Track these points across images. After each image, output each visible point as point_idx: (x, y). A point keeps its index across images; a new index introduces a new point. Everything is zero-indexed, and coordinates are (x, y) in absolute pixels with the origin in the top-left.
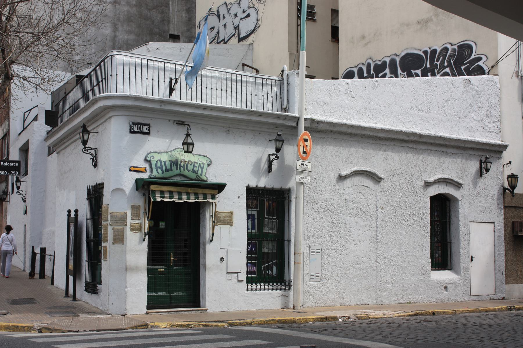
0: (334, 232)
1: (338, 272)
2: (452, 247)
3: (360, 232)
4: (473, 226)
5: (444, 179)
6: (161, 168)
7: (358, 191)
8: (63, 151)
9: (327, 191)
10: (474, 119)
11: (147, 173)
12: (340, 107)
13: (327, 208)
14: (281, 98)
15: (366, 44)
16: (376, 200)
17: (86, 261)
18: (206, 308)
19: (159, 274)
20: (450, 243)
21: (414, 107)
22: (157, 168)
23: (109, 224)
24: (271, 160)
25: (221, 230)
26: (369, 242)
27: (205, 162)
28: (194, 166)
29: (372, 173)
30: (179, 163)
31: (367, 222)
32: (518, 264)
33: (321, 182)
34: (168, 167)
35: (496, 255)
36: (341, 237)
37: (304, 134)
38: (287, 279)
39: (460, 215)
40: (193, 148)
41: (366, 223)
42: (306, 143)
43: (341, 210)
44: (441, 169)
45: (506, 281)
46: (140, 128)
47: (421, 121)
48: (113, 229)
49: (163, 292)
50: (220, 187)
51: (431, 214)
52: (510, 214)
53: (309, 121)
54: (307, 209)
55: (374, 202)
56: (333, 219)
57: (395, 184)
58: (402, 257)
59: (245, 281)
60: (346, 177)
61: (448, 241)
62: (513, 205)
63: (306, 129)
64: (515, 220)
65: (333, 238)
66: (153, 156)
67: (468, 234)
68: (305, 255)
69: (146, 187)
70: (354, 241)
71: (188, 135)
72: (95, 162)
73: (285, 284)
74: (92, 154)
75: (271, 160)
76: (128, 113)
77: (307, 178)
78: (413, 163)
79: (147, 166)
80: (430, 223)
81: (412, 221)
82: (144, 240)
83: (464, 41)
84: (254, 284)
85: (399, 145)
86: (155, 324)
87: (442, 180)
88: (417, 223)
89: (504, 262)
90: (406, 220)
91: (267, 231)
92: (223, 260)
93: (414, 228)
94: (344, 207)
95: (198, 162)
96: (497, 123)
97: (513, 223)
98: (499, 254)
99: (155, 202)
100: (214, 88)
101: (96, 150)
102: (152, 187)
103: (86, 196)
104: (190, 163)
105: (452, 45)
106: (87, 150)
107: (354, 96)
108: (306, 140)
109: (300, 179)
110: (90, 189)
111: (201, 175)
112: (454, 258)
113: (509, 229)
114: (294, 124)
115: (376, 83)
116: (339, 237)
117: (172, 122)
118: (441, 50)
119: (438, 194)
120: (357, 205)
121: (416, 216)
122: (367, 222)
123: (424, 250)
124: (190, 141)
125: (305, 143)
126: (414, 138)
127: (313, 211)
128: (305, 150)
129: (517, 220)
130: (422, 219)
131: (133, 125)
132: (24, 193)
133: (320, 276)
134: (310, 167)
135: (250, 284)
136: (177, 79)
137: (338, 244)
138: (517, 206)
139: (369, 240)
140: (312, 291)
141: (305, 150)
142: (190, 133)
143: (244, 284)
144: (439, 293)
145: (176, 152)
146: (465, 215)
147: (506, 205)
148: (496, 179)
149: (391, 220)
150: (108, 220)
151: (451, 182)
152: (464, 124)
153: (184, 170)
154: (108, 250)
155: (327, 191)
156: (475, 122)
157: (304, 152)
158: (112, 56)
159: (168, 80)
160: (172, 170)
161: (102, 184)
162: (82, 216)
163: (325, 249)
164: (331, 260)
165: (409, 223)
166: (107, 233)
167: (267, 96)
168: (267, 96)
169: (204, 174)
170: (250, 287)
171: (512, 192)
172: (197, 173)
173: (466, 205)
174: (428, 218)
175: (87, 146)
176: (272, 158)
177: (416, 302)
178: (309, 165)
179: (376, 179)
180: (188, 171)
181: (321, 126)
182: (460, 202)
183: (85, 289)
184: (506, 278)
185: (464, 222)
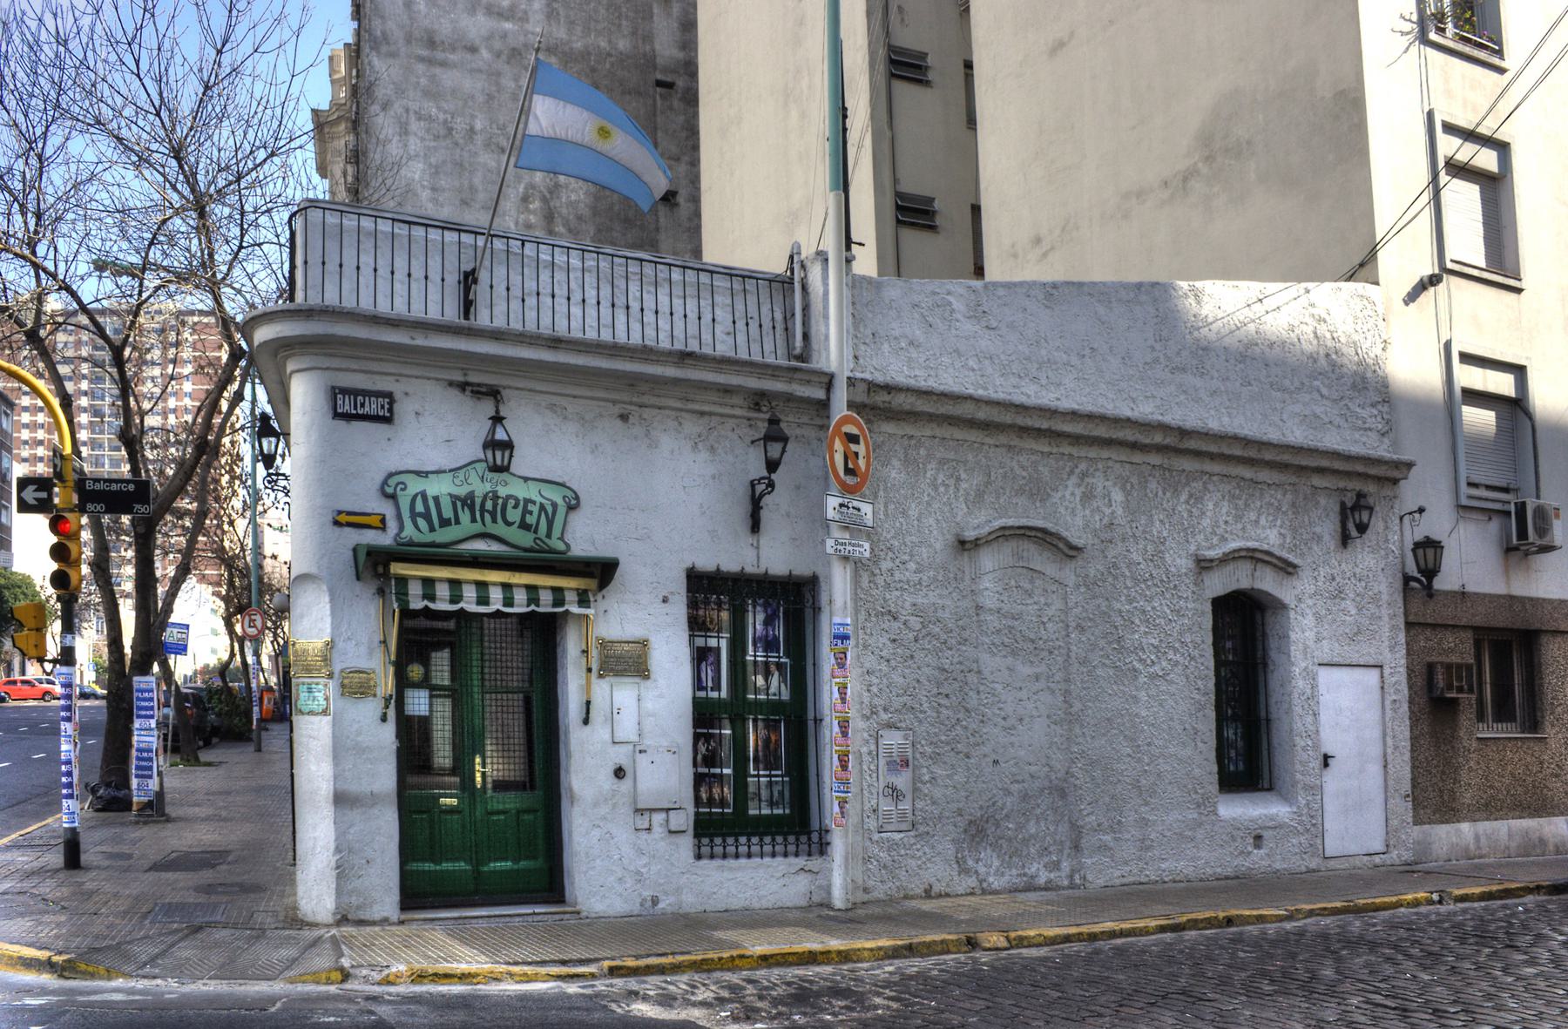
0: (947, 696)
1: (961, 805)
2: (1274, 731)
3: (1023, 694)
4: (1325, 675)
5: (1248, 550)
6: (427, 516)
10: (1322, 396)
11: (389, 530)
14: (786, 329)
15: (1045, 255)
18: (578, 908)
20: (1268, 720)
21: (1162, 360)
22: (414, 515)
24: (757, 494)
26: (1048, 722)
27: (560, 501)
28: (526, 512)
29: (1051, 534)
30: (478, 501)
31: (1042, 669)
32: (1443, 773)
33: (906, 557)
34: (448, 513)
35: (1389, 751)
36: (967, 710)
37: (845, 420)
38: (815, 825)
39: (1292, 648)
40: (511, 456)
41: (1038, 670)
42: (854, 447)
43: (966, 634)
44: (1240, 526)
45: (1414, 816)
46: (363, 405)
47: (1182, 397)
49: (457, 859)
50: (602, 572)
51: (1215, 644)
52: (1422, 644)
53: (862, 387)
54: (868, 631)
55: (1059, 613)
56: (944, 661)
57: (1115, 565)
58: (1139, 760)
59: (691, 831)
60: (976, 544)
61: (1263, 714)
62: (1429, 621)
63: (851, 405)
64: (1434, 659)
66: (402, 483)
67: (1313, 697)
68: (866, 758)
70: (1004, 719)
71: (497, 419)
73: (809, 839)
75: (757, 494)
76: (327, 362)
77: (859, 546)
78: (1165, 510)
80: (1213, 668)
81: (1164, 664)
84: (718, 840)
85: (1124, 458)
86: (394, 970)
87: (1243, 554)
88: (1179, 669)
89: (1408, 769)
90: (1149, 662)
93: (1171, 682)
94: (974, 626)
95: (539, 499)
96: (1380, 407)
97: (1431, 667)
98: (1396, 748)
100: (591, 301)
102: (398, 569)
107: (994, 325)
108: (853, 439)
109: (839, 547)
112: (1280, 759)
113: (1420, 681)
114: (820, 394)
116: (963, 710)
119: (1234, 592)
121: (1176, 651)
122: (1042, 669)
123: (1199, 739)
124: (500, 435)
125: (851, 445)
126: (1165, 438)
127: (884, 640)
128: (850, 466)
129: (1440, 659)
130: (1192, 658)
133: (910, 815)
134: (870, 516)
135: (705, 841)
138: (1440, 622)
139: (1048, 717)
141: (850, 466)
142: (502, 414)
143: (687, 843)
144: (1242, 853)
145: (473, 473)
146: (1306, 647)
147: (1412, 618)
148: (1383, 552)
149: (1107, 662)
151: (1267, 558)
152: (1297, 408)
156: (1325, 402)
157: (848, 471)
160: (458, 522)
163: (923, 742)
164: (939, 771)
165: (1157, 668)
167: (747, 324)
168: (747, 324)
170: (705, 850)
171: (1429, 587)
173: (1309, 621)
174: (1207, 655)
177: (1178, 878)
178: (867, 509)
180: (509, 524)
181: (901, 401)
182: (1292, 614)
184: (1414, 809)
185: (1303, 665)
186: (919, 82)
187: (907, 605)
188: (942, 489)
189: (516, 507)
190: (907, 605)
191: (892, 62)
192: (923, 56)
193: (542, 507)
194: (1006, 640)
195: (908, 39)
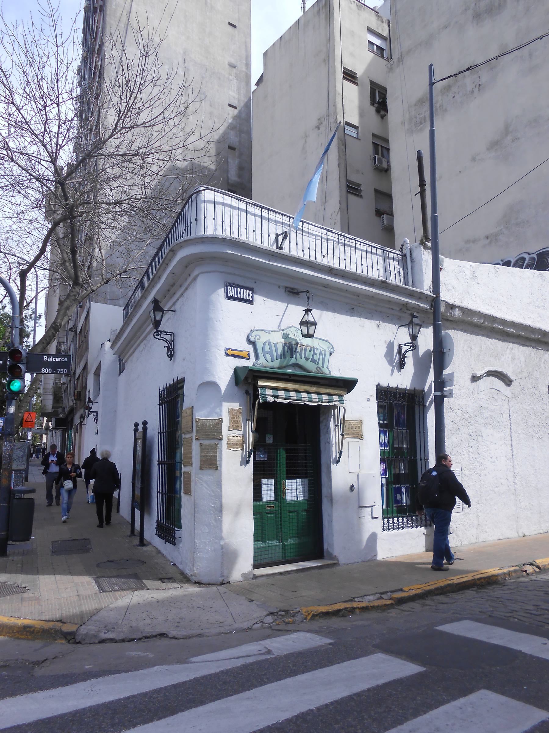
7: (491, 396)
8: (131, 358)
9: (462, 395)
12: (467, 294)
13: (463, 417)
16: (508, 407)
17: (158, 492)
19: (268, 513)
22: (264, 353)
23: (194, 438)
24: (403, 351)
25: (350, 444)
46: (240, 293)
48: (201, 445)
65: (472, 455)
66: (259, 336)
69: (250, 381)
72: (171, 352)
74: (166, 341)
79: (250, 348)
82: (248, 462)
83: (544, 249)
91: (397, 446)
92: (353, 488)
99: (266, 405)
101: (173, 334)
103: (157, 401)
104: (309, 348)
105: (529, 254)
106: (160, 335)
110: (163, 391)
111: (323, 366)
115: (497, 270)
117: (283, 290)
118: (517, 261)
120: (493, 414)
131: (230, 287)
132: (95, 414)
136: (286, 232)
137: (476, 462)
139: (506, 457)
140: (455, 526)
150: (192, 431)
153: (301, 358)
154: (193, 478)
155: (462, 395)
158: (197, 192)
159: (273, 237)
161: (183, 380)
162: (153, 430)
165: (539, 434)
166: (191, 453)
169: (326, 366)
172: (318, 364)
175: (160, 329)
176: (404, 349)
179: (507, 380)
180: (307, 359)
183: (157, 533)
186: (357, 195)
187: (457, 405)
188: (466, 353)
189: (310, 351)
190: (457, 405)
191: (348, 186)
192: (359, 185)
193: (321, 352)
194: (490, 422)
195: (354, 178)
